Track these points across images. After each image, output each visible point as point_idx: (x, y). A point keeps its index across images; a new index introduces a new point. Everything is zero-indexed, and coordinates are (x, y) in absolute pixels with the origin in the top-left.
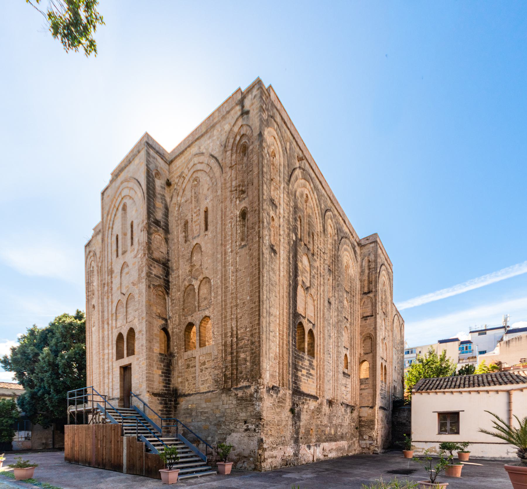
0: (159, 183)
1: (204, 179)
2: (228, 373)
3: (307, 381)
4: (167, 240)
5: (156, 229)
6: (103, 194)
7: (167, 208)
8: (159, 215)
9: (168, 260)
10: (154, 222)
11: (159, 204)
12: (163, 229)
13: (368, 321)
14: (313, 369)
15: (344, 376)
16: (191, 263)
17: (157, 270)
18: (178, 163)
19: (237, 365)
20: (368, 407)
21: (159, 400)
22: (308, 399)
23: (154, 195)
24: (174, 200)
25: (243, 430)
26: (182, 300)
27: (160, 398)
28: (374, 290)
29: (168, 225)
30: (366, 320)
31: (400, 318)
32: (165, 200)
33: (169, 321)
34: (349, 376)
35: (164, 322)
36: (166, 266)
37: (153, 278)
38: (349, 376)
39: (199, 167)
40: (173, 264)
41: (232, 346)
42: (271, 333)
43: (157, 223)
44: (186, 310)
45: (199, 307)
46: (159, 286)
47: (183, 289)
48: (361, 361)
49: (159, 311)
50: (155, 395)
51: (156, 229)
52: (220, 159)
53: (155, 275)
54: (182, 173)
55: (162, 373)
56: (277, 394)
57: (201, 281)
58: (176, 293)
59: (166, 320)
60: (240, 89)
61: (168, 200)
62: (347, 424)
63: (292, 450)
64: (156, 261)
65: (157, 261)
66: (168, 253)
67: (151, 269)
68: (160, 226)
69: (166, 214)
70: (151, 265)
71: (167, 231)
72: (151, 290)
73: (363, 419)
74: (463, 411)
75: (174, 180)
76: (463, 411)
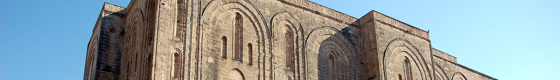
0: (113, 37)
1: (138, 28)
5: (105, 75)
6: (89, 44)
7: (119, 54)
8: (111, 62)
10: (103, 70)
11: (112, 52)
12: (113, 72)
18: (129, 17)
23: (108, 47)
28: (377, 75)
29: (119, 67)
32: (118, 48)
39: (137, 19)
43: (108, 69)
51: (105, 75)
52: (144, 13)
54: (129, 24)
61: (121, 46)
69: (118, 60)
71: (117, 72)
75: (126, 30)
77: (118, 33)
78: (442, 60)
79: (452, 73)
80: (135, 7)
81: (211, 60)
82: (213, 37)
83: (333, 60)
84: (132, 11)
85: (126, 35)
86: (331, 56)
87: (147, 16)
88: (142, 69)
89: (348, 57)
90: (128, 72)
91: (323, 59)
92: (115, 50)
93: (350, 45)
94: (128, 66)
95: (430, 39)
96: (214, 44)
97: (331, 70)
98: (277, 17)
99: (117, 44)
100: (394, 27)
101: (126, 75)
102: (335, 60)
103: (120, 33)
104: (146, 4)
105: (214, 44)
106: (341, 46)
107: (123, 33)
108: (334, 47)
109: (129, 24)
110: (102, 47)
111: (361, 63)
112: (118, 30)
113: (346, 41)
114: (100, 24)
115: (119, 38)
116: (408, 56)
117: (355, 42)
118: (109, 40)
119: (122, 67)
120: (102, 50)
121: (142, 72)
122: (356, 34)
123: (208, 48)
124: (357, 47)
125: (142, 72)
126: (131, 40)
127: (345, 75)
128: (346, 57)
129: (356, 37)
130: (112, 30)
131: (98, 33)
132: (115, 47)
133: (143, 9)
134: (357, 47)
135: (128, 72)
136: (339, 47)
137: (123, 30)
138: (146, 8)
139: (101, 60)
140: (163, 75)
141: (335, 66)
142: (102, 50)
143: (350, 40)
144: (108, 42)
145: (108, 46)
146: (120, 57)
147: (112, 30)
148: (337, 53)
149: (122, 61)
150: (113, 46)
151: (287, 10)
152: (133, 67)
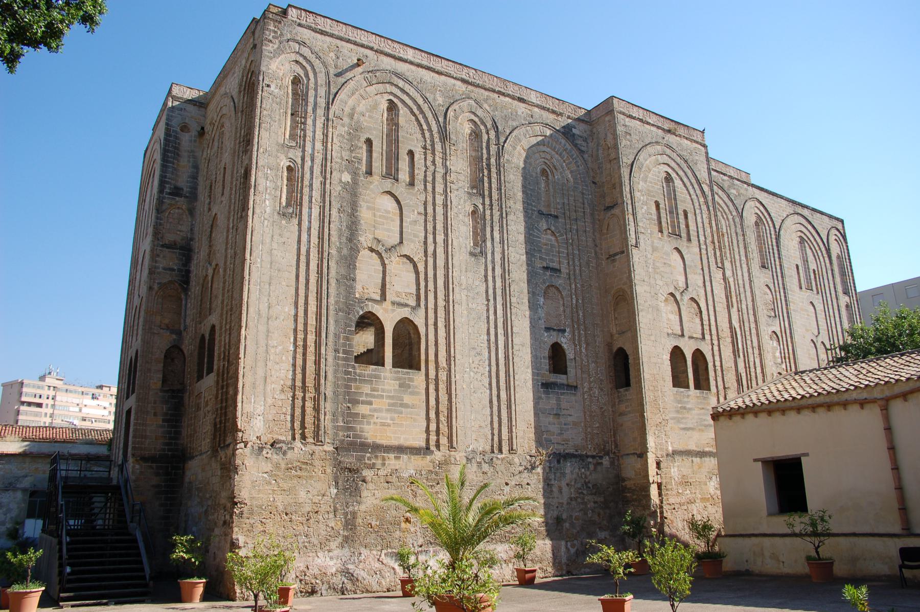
0: (186, 140)
1: (227, 124)
2: (218, 420)
3: (392, 419)
4: (191, 212)
5: (173, 202)
7: (196, 167)
8: (183, 182)
9: (192, 239)
10: (170, 194)
11: (184, 166)
12: (186, 197)
13: (617, 264)
14: (412, 393)
15: (547, 393)
16: (210, 241)
17: (170, 260)
18: (212, 107)
19: (226, 407)
20: (634, 454)
21: (151, 467)
22: (392, 456)
24: (205, 153)
25: (222, 522)
26: (200, 298)
27: (154, 465)
29: (196, 189)
30: (614, 261)
31: (816, 219)
32: (194, 157)
33: (184, 334)
34: (576, 387)
35: (174, 336)
36: (186, 251)
37: (159, 273)
38: (576, 387)
40: (195, 245)
41: (223, 375)
42: (273, 350)
43: (177, 192)
44: (203, 314)
45: (210, 309)
46: (170, 282)
47: (201, 281)
48: (615, 350)
49: (166, 321)
50: (144, 459)
51: (173, 202)
52: (236, 101)
53: (164, 269)
54: (213, 118)
55: (164, 421)
56: (285, 453)
57: (214, 270)
58: (195, 288)
59: (179, 333)
60: (254, 19)
62: (565, 500)
63: (332, 563)
64: (167, 248)
65: (171, 246)
66: (191, 230)
67: (156, 262)
68: (180, 195)
69: (194, 177)
70: (158, 256)
71: (193, 196)
72: (154, 293)
73: (628, 484)
74: (806, 455)
75: (208, 128)
76: (806, 455)
77: (194, 133)
78: (726, 178)
79: (743, 199)
80: (222, 90)
81: (347, 177)
82: (350, 140)
83: (547, 177)
84: (217, 97)
85: (207, 136)
86: (544, 172)
87: (241, 105)
88: (233, 192)
89: (571, 172)
90: (210, 196)
91: (532, 176)
92: (189, 161)
93: (575, 153)
94: (211, 186)
95: (707, 143)
96: (351, 151)
97: (543, 195)
98: (455, 106)
99: (192, 151)
100: (648, 123)
101: (207, 201)
102: (550, 177)
103: (197, 133)
104: (240, 85)
105: (351, 151)
106: (560, 155)
107: (202, 132)
108: (549, 157)
109: (213, 118)
110: (168, 157)
111: (594, 183)
112: (194, 128)
113: (568, 147)
114: (164, 118)
115: (195, 141)
116: (670, 171)
117: (583, 148)
118: (179, 144)
119: (200, 188)
120: (167, 161)
121: (233, 197)
122: (585, 135)
123: (342, 158)
124: (586, 156)
125: (233, 197)
126: (216, 144)
127: (566, 201)
128: (568, 172)
129: (585, 140)
130: (185, 128)
131: (161, 133)
132: (189, 157)
133: (235, 93)
134: (586, 156)
135: (210, 196)
136: (557, 156)
137: (203, 128)
138: (240, 92)
139: (165, 177)
140: (267, 202)
141: (551, 187)
142: (167, 161)
143: (576, 145)
144: (177, 149)
145: (178, 155)
146: (197, 173)
147: (185, 128)
148: (554, 166)
149: (201, 179)
150: (186, 154)
151: (472, 95)
152: (218, 189)
